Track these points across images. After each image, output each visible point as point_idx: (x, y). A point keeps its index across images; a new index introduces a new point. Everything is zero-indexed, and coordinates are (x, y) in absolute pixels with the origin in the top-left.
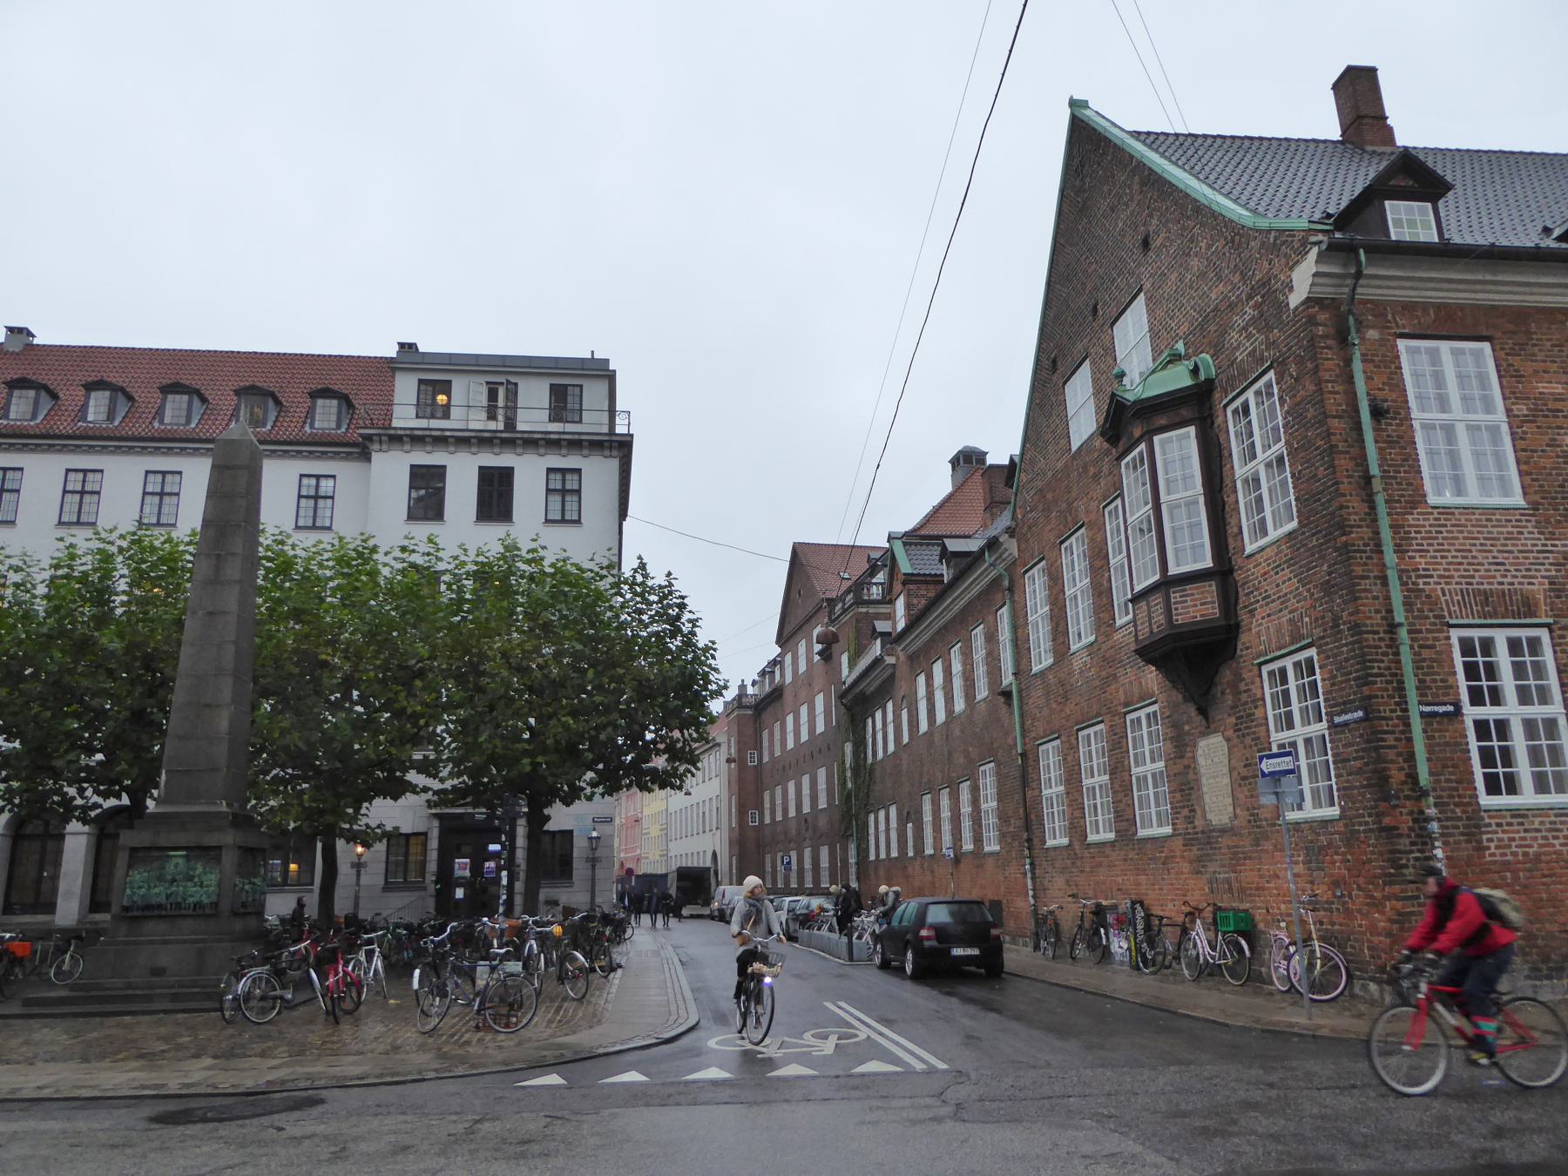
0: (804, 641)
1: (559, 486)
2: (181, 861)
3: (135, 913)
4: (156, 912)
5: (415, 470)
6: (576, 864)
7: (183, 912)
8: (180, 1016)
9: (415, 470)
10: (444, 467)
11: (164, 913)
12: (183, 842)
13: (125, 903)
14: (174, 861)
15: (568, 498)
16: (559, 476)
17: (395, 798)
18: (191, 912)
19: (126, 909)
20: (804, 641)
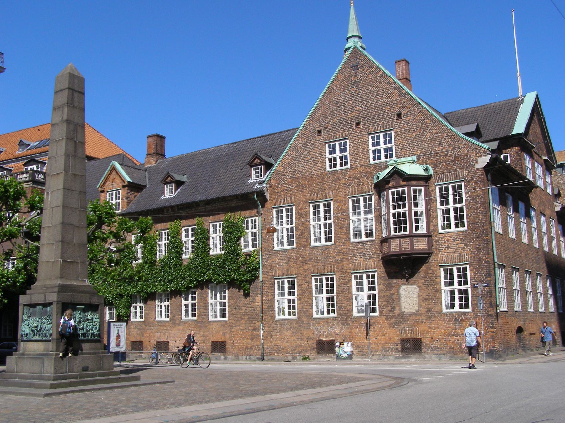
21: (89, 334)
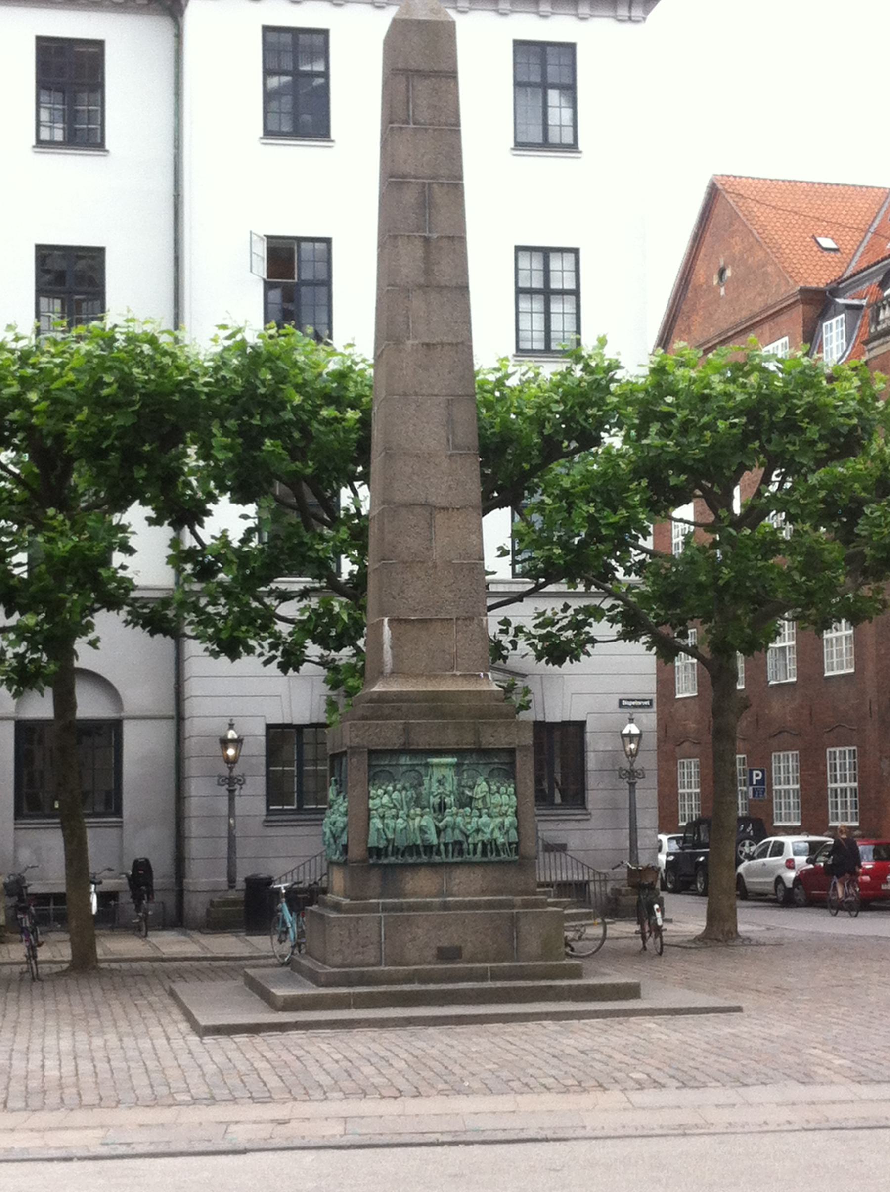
0: (186, 526)
1: (538, 284)
2: (449, 773)
3: (392, 859)
4: (424, 858)
5: (272, 37)
6: (592, 781)
7: (467, 857)
8: (209, 955)
9: (273, 37)
10: (99, 44)
11: (437, 859)
12: (451, 739)
13: (373, 841)
14: (437, 774)
15: (556, 307)
16: (537, 263)
17: (152, 633)
18: (478, 857)
19: (377, 852)
20: (186, 526)
21: (475, 845)
